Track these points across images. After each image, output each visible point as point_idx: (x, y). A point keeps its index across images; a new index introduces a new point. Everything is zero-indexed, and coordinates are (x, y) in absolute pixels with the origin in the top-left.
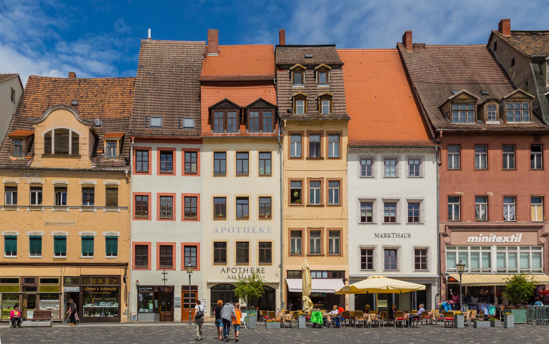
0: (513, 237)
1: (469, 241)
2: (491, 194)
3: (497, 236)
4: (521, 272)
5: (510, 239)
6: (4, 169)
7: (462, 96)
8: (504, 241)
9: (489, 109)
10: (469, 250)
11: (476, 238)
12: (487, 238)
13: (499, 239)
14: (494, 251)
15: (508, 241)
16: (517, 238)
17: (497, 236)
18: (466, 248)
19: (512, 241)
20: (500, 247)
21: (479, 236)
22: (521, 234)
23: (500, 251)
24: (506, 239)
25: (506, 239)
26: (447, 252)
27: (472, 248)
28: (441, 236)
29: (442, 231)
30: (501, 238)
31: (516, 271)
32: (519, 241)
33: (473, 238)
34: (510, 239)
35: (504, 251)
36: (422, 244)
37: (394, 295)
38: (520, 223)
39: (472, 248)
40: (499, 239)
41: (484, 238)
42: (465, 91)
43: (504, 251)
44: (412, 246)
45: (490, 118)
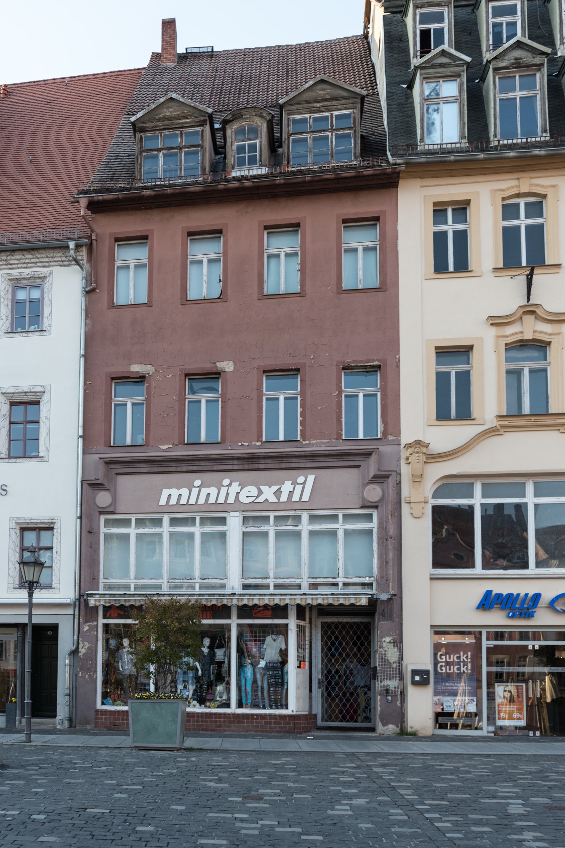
0: (287, 486)
1: (163, 501)
2: (228, 366)
3: (242, 486)
4: (276, 586)
5: (278, 493)
6: (319, 578)
7: (167, 112)
8: (261, 499)
9: (240, 137)
10: (166, 529)
11: (184, 492)
12: (213, 491)
13: (248, 494)
14: (234, 525)
15: (273, 499)
16: (300, 487)
17: (242, 486)
18: (158, 522)
19: (284, 498)
20: (254, 516)
21: (191, 488)
22: (311, 479)
23: (250, 529)
24: (268, 493)
25: (268, 493)
26: (107, 536)
27: (174, 522)
28: (91, 486)
29: (99, 474)
30: (253, 491)
31: (299, 587)
32: (306, 498)
33: (175, 493)
34: (278, 493)
35: (264, 528)
36: (37, 513)
37: (449, 728)
38: (309, 445)
39: (174, 522)
40: (248, 494)
41: (205, 491)
42: (174, 96)
43: (264, 528)
44: (11, 519)
45: (241, 162)
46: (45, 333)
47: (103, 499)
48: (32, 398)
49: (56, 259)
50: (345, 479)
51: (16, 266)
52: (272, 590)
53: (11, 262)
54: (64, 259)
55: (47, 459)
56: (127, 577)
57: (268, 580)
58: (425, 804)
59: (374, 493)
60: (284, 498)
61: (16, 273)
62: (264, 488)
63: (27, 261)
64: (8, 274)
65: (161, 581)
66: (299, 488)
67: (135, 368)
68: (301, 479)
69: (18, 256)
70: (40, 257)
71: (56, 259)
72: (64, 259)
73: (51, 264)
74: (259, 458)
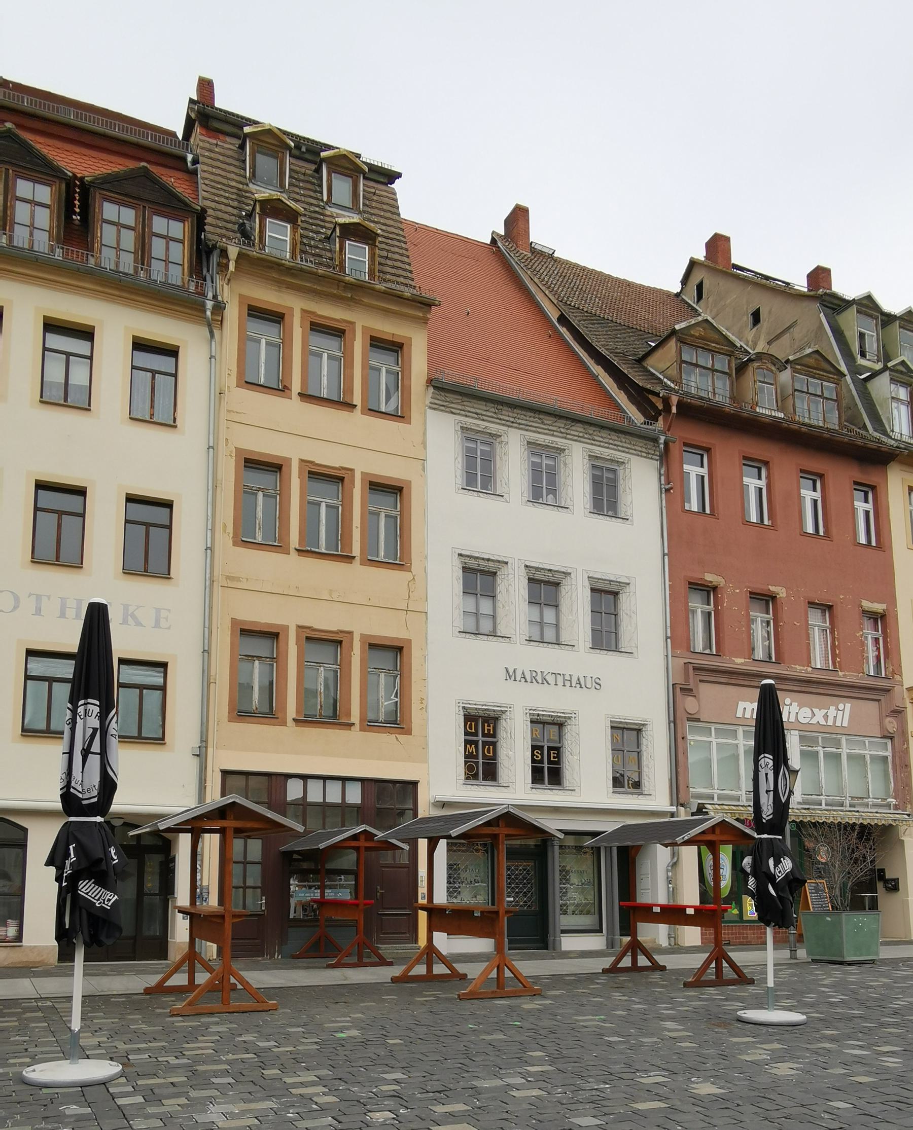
0: (832, 712)
1: (739, 714)
3: (801, 706)
5: (826, 717)
8: (814, 721)
17: (801, 706)
28: (680, 691)
32: (845, 724)
34: (826, 717)
36: (630, 714)
46: (627, 522)
47: (690, 704)
48: (614, 588)
49: (637, 448)
50: (870, 709)
51: (598, 443)
52: (716, 801)
53: (596, 438)
54: (644, 450)
55: (635, 654)
56: (711, 786)
57: (821, 797)
58: (220, 1062)
59: (891, 725)
60: (830, 723)
61: (598, 451)
62: (816, 711)
63: (611, 441)
64: (590, 451)
65: (740, 793)
66: (840, 713)
67: (709, 577)
68: (841, 706)
69: (604, 433)
70: (623, 441)
71: (637, 448)
72: (644, 450)
73: (568, 436)
74: (814, 682)
